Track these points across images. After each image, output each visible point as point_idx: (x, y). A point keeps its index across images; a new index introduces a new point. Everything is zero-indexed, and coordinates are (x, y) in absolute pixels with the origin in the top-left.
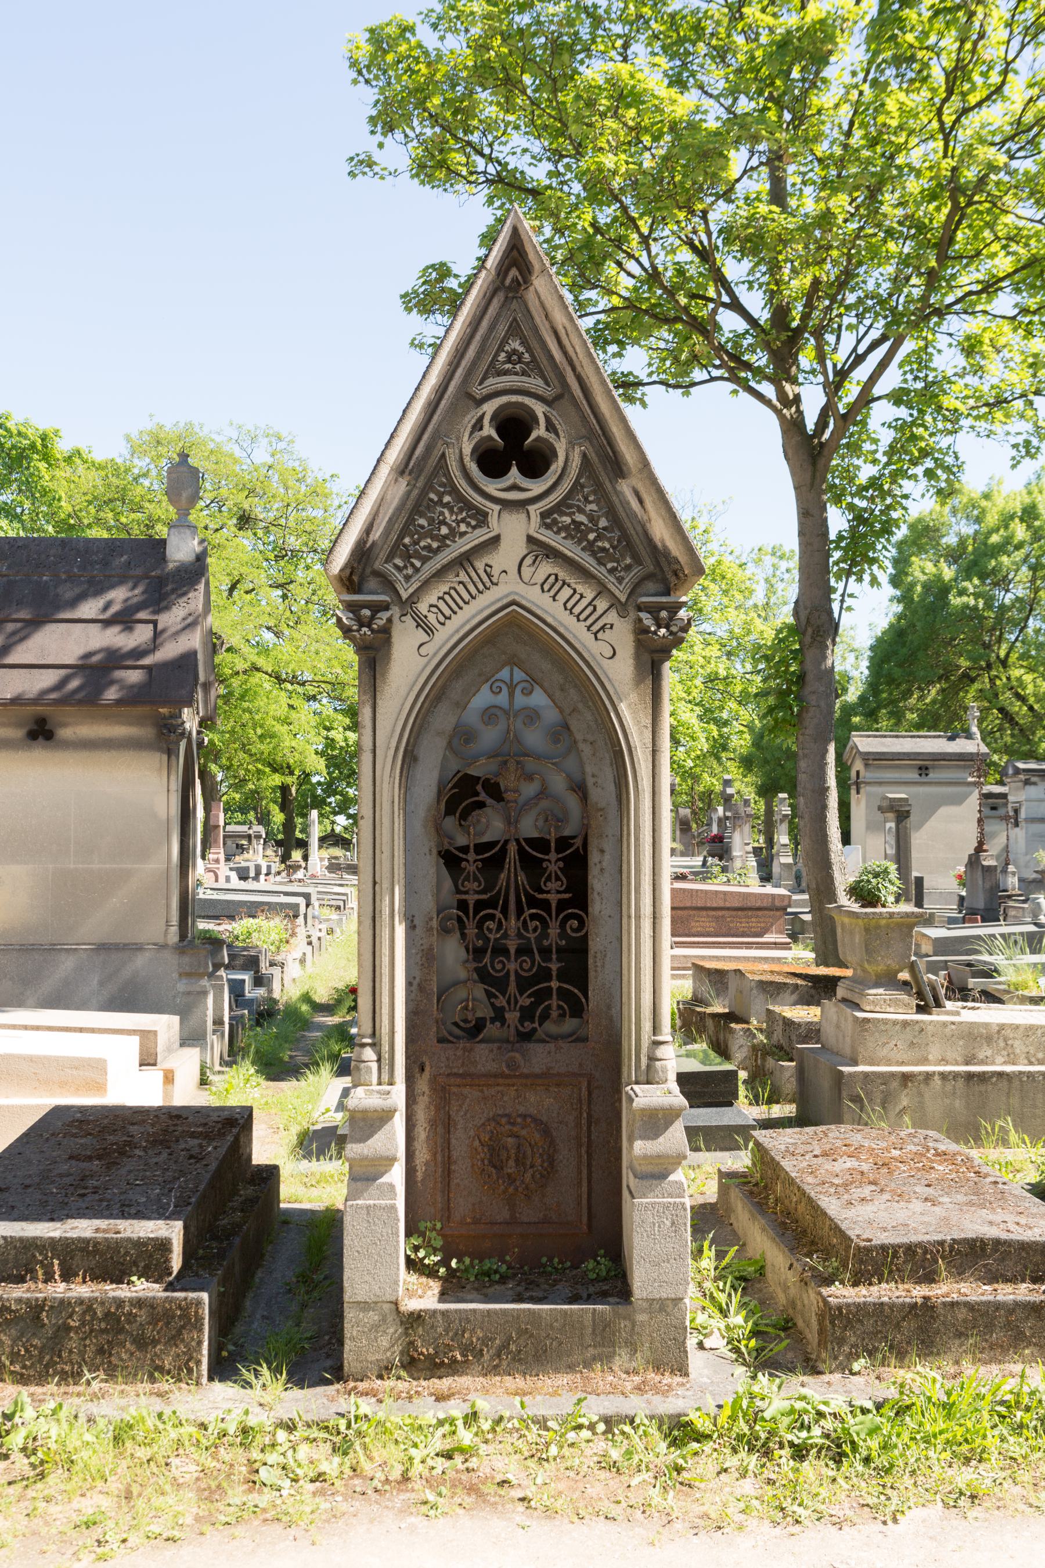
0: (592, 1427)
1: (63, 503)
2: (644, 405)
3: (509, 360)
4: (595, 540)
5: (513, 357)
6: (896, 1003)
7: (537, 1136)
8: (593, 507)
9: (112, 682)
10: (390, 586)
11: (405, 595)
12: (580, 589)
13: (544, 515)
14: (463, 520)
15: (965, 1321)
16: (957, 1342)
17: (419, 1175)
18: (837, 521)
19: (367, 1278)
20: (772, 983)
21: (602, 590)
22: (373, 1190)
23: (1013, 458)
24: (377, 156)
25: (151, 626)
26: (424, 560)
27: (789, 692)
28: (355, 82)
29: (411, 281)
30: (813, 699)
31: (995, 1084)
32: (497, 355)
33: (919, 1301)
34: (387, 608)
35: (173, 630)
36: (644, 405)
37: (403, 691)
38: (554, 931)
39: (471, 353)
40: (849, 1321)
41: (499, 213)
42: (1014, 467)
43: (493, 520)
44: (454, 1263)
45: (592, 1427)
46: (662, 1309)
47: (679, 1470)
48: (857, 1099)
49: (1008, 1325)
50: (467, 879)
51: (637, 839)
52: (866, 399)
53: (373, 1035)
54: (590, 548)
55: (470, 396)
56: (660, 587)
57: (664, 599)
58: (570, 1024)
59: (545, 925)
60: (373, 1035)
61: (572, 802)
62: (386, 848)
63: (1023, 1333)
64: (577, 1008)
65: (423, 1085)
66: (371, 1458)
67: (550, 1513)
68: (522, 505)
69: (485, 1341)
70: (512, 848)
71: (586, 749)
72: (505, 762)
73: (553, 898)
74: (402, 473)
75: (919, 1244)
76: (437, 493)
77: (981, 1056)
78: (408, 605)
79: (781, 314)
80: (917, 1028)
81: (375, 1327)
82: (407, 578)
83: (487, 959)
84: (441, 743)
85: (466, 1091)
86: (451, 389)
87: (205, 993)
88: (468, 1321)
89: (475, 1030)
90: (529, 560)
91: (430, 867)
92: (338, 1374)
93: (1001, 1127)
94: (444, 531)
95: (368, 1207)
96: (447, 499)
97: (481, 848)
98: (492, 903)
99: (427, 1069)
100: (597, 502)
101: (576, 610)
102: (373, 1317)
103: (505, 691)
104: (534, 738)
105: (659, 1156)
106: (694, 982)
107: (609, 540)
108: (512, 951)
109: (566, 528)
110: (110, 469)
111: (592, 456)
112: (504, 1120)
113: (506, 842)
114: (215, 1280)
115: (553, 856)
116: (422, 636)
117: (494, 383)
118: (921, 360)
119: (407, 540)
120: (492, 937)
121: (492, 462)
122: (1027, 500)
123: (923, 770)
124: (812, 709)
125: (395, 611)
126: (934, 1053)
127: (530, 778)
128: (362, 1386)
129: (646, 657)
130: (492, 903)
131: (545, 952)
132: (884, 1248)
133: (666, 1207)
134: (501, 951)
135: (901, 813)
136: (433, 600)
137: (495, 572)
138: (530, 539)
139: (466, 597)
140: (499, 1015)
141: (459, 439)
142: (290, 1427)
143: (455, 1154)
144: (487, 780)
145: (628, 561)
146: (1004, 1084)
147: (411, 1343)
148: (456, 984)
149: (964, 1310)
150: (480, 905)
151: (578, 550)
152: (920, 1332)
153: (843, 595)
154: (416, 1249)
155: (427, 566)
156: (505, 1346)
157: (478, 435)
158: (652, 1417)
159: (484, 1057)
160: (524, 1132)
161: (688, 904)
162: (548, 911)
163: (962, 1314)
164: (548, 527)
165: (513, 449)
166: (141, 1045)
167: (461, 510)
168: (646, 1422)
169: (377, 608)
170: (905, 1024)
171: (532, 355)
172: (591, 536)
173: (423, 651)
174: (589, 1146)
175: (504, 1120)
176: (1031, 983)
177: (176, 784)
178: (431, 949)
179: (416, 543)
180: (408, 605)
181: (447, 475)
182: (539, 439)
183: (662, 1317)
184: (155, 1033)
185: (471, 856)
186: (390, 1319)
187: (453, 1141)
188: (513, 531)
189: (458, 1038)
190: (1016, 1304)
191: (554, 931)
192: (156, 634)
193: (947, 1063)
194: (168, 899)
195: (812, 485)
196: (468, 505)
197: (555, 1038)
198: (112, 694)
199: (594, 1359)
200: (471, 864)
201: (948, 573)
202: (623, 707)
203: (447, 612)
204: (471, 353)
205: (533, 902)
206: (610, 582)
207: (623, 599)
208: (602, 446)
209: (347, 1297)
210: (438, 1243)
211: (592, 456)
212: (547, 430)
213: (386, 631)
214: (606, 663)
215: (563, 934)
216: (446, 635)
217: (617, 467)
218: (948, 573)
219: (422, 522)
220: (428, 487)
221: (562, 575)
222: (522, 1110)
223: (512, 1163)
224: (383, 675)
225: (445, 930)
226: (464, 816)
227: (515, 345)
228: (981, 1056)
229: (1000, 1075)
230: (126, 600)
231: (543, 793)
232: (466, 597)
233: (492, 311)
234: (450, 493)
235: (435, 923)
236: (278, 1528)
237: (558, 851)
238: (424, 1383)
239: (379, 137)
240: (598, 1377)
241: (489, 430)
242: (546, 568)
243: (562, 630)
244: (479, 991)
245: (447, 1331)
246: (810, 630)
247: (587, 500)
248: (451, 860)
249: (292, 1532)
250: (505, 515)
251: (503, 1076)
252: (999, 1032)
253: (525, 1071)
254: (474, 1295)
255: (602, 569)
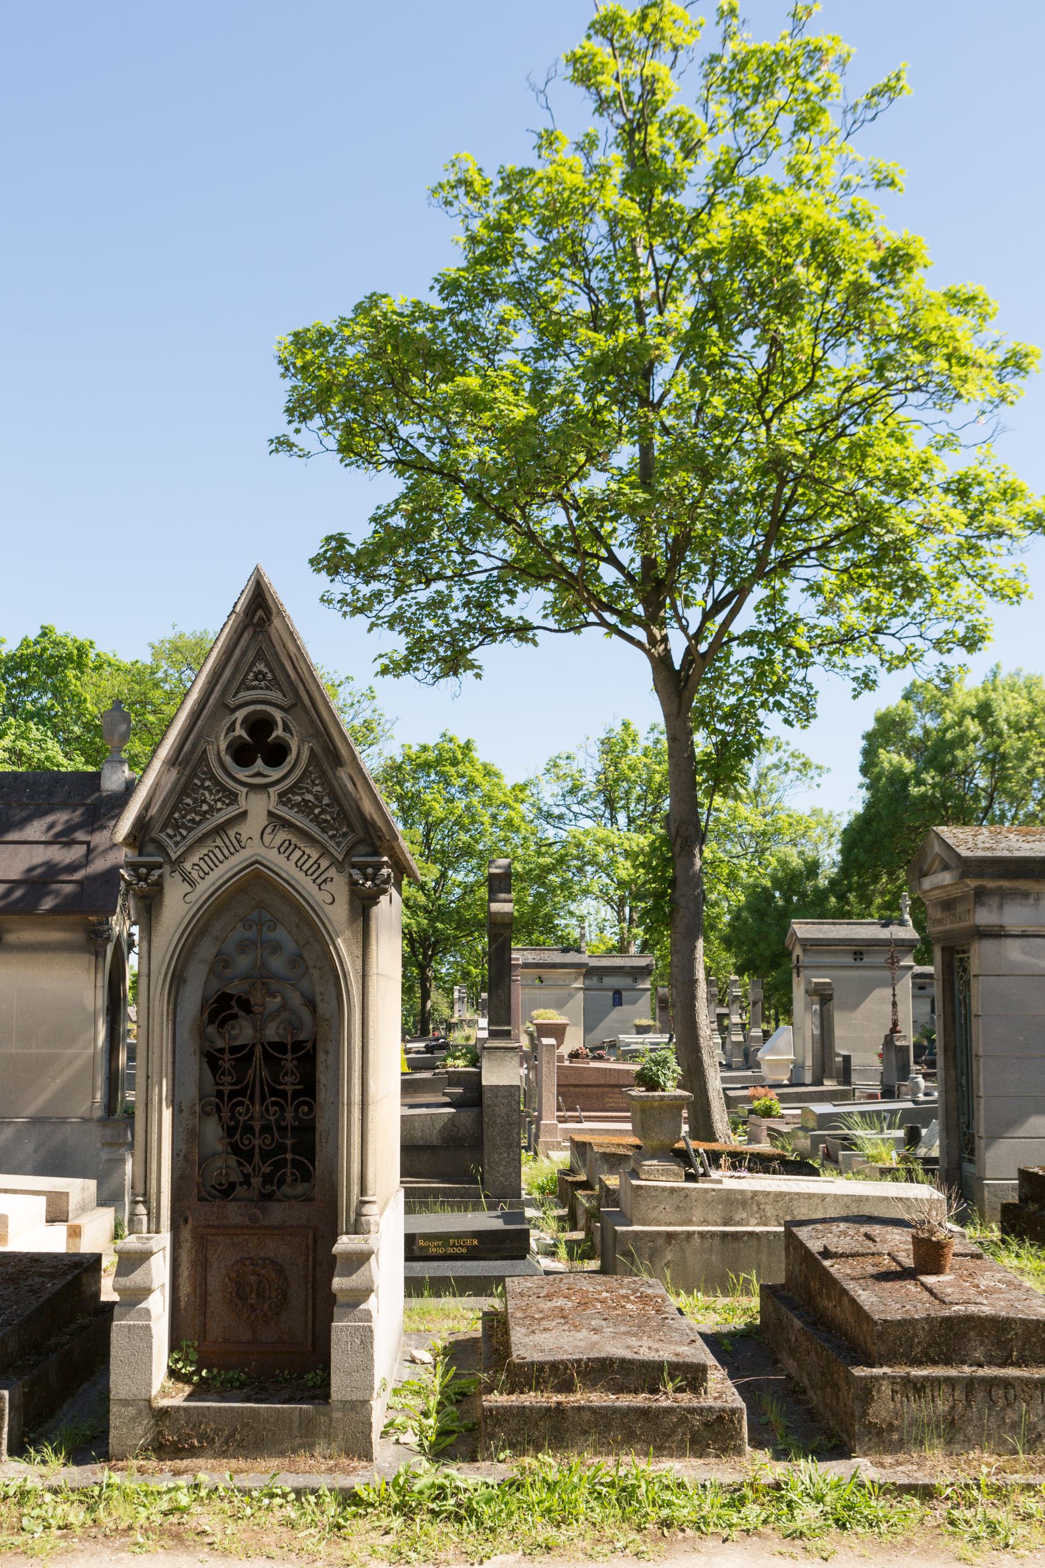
0: (284, 1496)
1: (88, 705)
2: (536, 644)
3: (256, 679)
4: (320, 813)
5: (259, 676)
6: (666, 1172)
7: (273, 1274)
8: (319, 788)
9: (50, 893)
10: (162, 849)
11: (174, 857)
12: (308, 851)
13: (280, 795)
14: (219, 800)
15: (589, 1421)
16: (582, 1438)
17: (183, 1304)
18: (702, 742)
19: (128, 1381)
20: (614, 1155)
21: (325, 852)
22: (133, 1313)
23: (855, 690)
24: (293, 438)
25: (85, 847)
26: (190, 830)
27: (664, 894)
28: (283, 376)
29: (315, 549)
30: (682, 902)
31: (746, 1242)
32: (247, 674)
33: (553, 1405)
34: (160, 866)
35: (101, 849)
36: (536, 644)
37: (172, 930)
38: (289, 1115)
39: (227, 673)
40: (498, 1420)
41: (409, 482)
42: (855, 697)
43: (242, 800)
44: (204, 1373)
45: (284, 1496)
46: (353, 1408)
47: (339, 1527)
48: (627, 1254)
49: (624, 1427)
50: (223, 1073)
51: (349, 1043)
52: (718, 644)
53: (145, 1195)
54: (316, 820)
55: (228, 707)
56: (369, 849)
57: (370, 859)
58: (301, 1188)
59: (283, 1110)
60: (145, 1195)
61: (305, 1014)
62: (156, 1051)
63: (634, 1432)
64: (306, 1175)
65: (186, 1234)
66: (110, 1514)
67: (226, 1553)
68: (265, 787)
69: (216, 1431)
70: (258, 1050)
71: (316, 973)
72: (253, 984)
73: (289, 1089)
74: (173, 765)
75: (562, 1362)
76: (200, 779)
77: (737, 1218)
78: (177, 864)
79: (649, 563)
80: (682, 1194)
81: (133, 1419)
82: (177, 844)
83: (237, 1137)
84: (204, 969)
85: (220, 1239)
86: (212, 700)
87: (123, 1161)
88: (204, 1416)
89: (227, 1191)
90: (269, 830)
91: (193, 1065)
92: (105, 1456)
93: (745, 1279)
94: (205, 807)
95: (129, 1326)
96: (207, 783)
97: (234, 1050)
98: (242, 1093)
99: (190, 1221)
100: (322, 785)
101: (305, 867)
102: (132, 1411)
103: (255, 928)
104: (277, 964)
105: (352, 1290)
106: (572, 1154)
107: (330, 814)
108: (257, 1130)
109: (298, 805)
110: (137, 675)
111: (319, 750)
112: (248, 1262)
113: (254, 1045)
114: (20, 1383)
115: (289, 1056)
116: (187, 888)
117: (245, 695)
118: (773, 603)
119: (176, 815)
120: (242, 1119)
121: (242, 754)
122: (982, 696)
123: (858, 955)
124: (682, 911)
125: (167, 868)
126: (697, 1214)
127: (273, 996)
128: (120, 1464)
129: (358, 903)
130: (242, 1093)
131: (282, 1129)
132: (532, 1363)
133: (357, 1329)
134: (248, 1129)
135: (824, 996)
136: (196, 860)
137: (243, 839)
138: (270, 814)
139: (221, 857)
140: (247, 1180)
141: (217, 738)
142: (56, 1492)
143: (210, 1288)
144: (240, 997)
145: (345, 829)
146: (754, 1242)
147: (160, 1432)
148: (214, 1155)
149: (588, 1413)
150: (233, 1094)
151: (307, 821)
152: (555, 1430)
153: (709, 810)
154: (177, 1361)
155: (191, 835)
156: (232, 1435)
157: (232, 735)
158: (330, 1490)
159: (234, 1212)
160: (263, 1272)
161: (602, 1082)
162: (285, 1099)
163: (587, 1416)
164: (284, 804)
165: (259, 745)
166: (48, 1205)
167: (218, 792)
168: (327, 1493)
169: (152, 867)
170: (673, 1190)
171: (273, 674)
172: (317, 811)
173: (187, 899)
174: (314, 1282)
175: (248, 1262)
176: (884, 1155)
177: (103, 981)
178: (194, 1128)
179: (184, 817)
180: (177, 864)
181: (208, 766)
182: (278, 737)
183: (352, 1415)
184: (67, 1194)
185: (227, 1056)
186: (144, 1413)
187: (209, 1278)
188: (258, 808)
189: (214, 1197)
190: (629, 1408)
191: (289, 1115)
192: (89, 851)
193: (708, 1224)
194: (94, 1079)
195: (679, 713)
196: (224, 788)
197: (288, 1198)
198: (47, 904)
199: (300, 1446)
200: (226, 1062)
201: (909, 766)
202: (339, 941)
203: (207, 869)
204: (227, 673)
205: (274, 1092)
206: (331, 845)
207: (340, 858)
208: (325, 743)
209: (112, 1397)
210: (194, 1357)
211: (319, 750)
212: (284, 730)
213: (159, 885)
214: (327, 908)
215: (296, 1117)
216: (205, 887)
217: (337, 760)
218: (909, 766)
219: (189, 801)
220: (193, 775)
221: (294, 841)
222: (262, 1254)
223: (254, 1296)
224: (157, 917)
225: (205, 1114)
226: (221, 1025)
227: (261, 667)
228: (737, 1218)
229: (751, 1234)
230: (67, 822)
231: (284, 1007)
232: (221, 857)
233: (243, 642)
234: (210, 779)
235: (197, 1108)
236: (23, 1558)
237: (294, 1052)
238: (168, 1463)
239: (296, 425)
240: (302, 1461)
241: (240, 731)
242: (282, 836)
243: (293, 882)
244: (232, 1161)
245: (187, 1423)
246: (679, 841)
247: (314, 784)
248: (211, 1059)
249: (32, 1561)
250: (251, 795)
251: (247, 1227)
252: (752, 1198)
253: (265, 1223)
254: (215, 1396)
255: (325, 836)
